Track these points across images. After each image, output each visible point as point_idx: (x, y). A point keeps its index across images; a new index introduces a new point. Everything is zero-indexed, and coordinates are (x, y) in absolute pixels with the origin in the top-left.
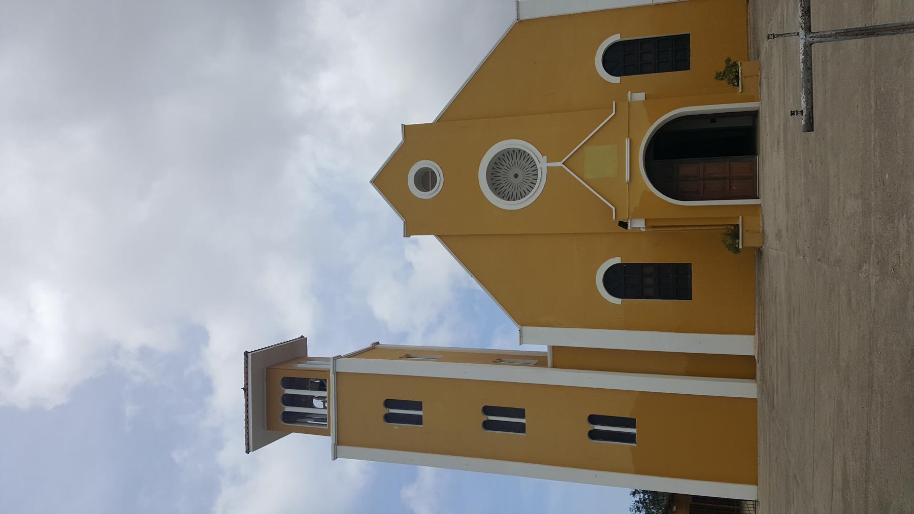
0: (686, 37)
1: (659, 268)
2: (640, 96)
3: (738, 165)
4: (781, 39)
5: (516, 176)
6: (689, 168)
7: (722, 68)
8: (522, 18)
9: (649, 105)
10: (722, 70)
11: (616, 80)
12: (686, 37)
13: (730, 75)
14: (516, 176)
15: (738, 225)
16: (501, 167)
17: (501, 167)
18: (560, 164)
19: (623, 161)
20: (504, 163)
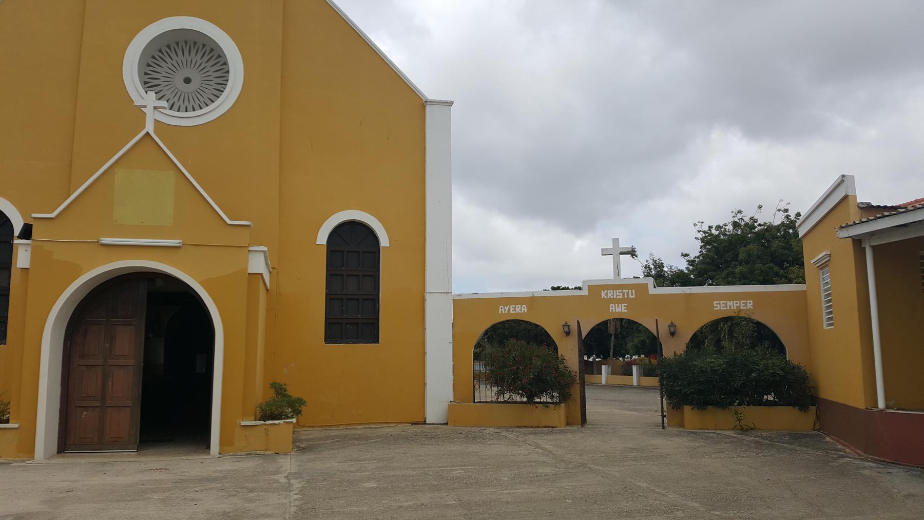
0: (375, 339)
1: (371, 301)
2: (257, 264)
3: (126, 419)
4: (489, 400)
5: (187, 81)
6: (126, 345)
7: (294, 392)
8: (428, 108)
9: (251, 283)
10: (289, 393)
11: (322, 238)
12: (375, 339)
13: (279, 406)
14: (187, 81)
15: (7, 421)
16: (206, 58)
17: (206, 58)
18: (150, 128)
19: (139, 231)
20: (211, 63)
